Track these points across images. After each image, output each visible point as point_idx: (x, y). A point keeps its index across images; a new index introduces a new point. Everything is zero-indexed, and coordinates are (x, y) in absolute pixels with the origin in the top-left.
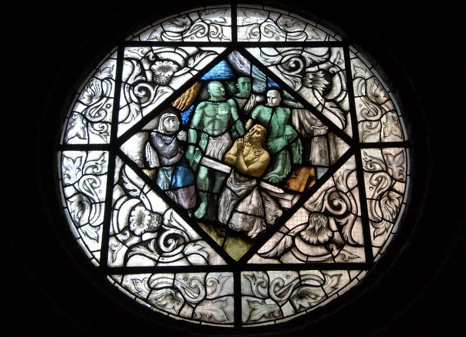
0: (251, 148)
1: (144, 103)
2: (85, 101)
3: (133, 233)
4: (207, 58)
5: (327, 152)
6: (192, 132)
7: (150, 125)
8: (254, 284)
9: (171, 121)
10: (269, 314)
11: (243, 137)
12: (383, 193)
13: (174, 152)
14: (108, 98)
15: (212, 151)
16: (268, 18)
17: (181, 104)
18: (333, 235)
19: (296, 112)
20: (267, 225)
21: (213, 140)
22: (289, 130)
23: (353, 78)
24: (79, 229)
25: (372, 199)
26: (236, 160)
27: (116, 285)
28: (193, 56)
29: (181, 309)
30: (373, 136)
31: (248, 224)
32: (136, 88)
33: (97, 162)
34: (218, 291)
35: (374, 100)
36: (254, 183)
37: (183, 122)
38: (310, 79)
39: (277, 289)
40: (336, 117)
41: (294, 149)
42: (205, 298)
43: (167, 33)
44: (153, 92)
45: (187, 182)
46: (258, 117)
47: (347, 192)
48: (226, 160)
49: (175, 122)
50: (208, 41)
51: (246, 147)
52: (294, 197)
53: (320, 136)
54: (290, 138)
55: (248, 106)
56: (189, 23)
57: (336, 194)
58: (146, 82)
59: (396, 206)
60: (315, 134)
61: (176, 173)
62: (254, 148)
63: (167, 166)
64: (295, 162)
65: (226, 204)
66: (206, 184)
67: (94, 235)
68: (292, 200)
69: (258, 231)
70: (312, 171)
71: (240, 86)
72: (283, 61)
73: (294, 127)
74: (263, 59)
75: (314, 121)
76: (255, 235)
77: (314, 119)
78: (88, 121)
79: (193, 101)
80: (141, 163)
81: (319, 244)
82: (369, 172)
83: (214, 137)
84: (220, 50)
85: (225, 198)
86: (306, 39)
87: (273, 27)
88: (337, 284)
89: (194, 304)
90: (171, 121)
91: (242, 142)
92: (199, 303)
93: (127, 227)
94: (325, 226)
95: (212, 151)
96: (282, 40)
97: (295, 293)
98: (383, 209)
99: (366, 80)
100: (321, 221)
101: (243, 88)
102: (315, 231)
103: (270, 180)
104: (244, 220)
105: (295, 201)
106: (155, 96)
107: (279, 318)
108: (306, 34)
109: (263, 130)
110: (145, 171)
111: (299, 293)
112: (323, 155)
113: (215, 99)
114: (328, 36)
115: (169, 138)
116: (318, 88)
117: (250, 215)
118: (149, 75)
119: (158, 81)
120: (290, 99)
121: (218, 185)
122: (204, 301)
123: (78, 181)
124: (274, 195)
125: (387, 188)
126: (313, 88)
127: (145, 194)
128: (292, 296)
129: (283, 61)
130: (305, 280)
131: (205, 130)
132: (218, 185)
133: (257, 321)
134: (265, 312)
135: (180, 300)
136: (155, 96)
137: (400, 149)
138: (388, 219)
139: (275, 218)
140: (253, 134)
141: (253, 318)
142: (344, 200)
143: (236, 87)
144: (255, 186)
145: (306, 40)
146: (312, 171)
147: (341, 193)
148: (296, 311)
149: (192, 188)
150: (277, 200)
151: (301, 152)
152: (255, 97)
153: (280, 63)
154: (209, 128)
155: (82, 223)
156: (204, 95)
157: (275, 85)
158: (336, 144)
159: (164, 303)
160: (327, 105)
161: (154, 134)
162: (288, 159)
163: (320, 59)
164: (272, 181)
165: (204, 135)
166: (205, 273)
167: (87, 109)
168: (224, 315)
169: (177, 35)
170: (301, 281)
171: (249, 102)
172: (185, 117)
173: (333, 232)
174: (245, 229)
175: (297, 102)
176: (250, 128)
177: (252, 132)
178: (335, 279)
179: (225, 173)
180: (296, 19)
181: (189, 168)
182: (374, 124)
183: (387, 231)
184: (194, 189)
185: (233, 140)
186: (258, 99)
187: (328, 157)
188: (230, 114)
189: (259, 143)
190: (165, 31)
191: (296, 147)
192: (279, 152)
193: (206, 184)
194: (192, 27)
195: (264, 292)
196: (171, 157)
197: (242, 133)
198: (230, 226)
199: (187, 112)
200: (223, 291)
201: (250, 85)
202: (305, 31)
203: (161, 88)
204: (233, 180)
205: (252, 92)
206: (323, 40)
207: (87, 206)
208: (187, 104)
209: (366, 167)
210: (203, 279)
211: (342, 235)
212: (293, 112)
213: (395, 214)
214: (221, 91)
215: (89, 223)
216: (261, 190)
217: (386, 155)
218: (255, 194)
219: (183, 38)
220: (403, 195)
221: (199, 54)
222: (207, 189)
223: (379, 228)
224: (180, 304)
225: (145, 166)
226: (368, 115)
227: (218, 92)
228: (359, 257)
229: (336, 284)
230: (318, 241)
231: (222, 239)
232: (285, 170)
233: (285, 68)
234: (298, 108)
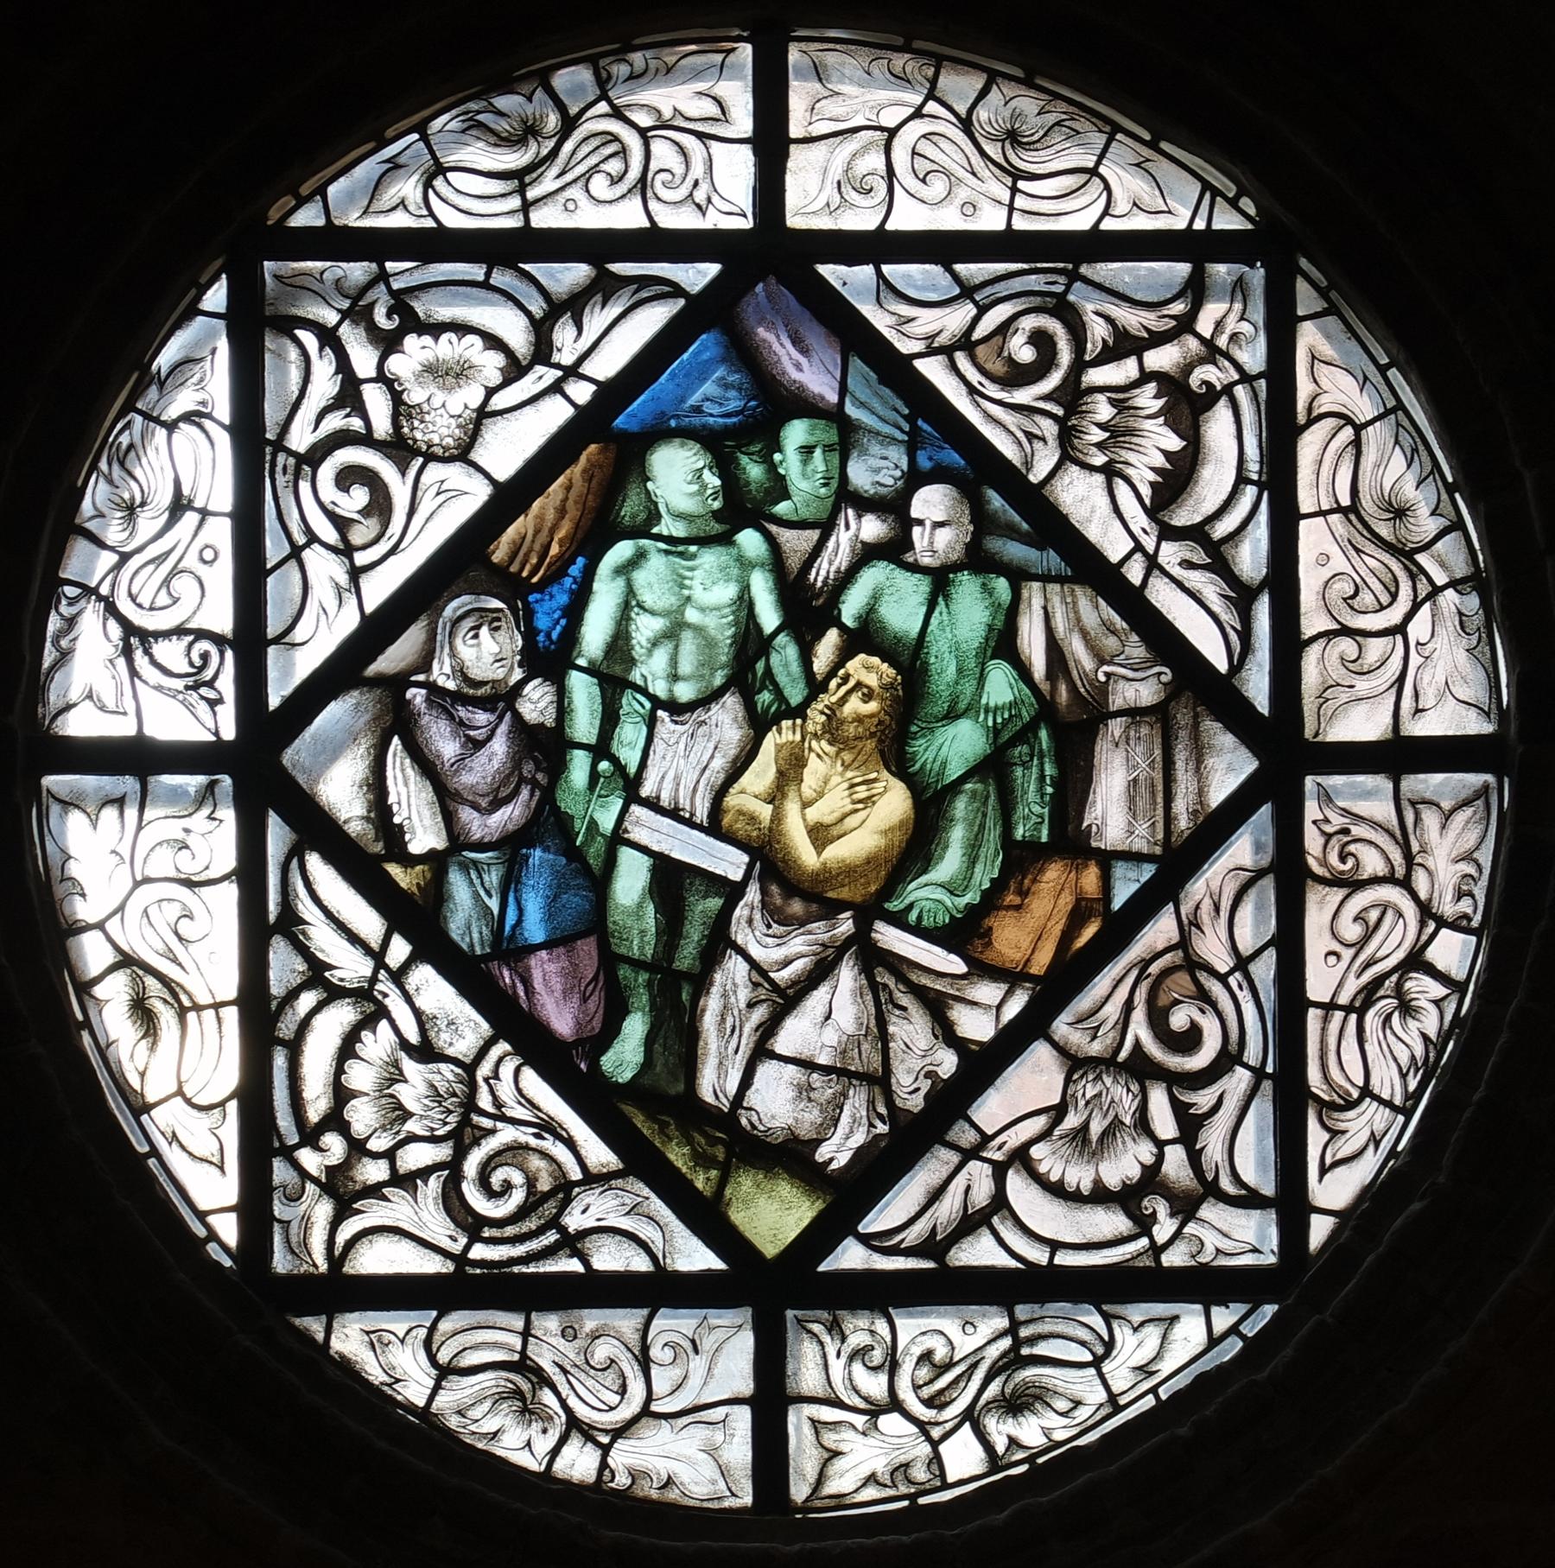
0: (833, 765)
1: (364, 547)
5: (1160, 787)
6: (582, 689)
7: (391, 660)
9: (484, 631)
10: (892, 1474)
11: (800, 712)
12: (1379, 981)
13: (505, 781)
14: (205, 513)
15: (671, 775)
16: (931, 96)
17: (530, 550)
18: (1160, 1158)
19: (1034, 593)
20: (895, 1114)
21: (673, 727)
22: (1000, 686)
23: (1301, 418)
24: (1123, 1401)
25: (1329, 1007)
26: (772, 821)
28: (573, 306)
29: (555, 1452)
30: (1362, 708)
31: (816, 1112)
32: (327, 471)
34: (695, 1381)
35: (1384, 530)
36: (846, 925)
37: (541, 638)
38: (1099, 425)
40: (1202, 612)
41: (1019, 772)
42: (646, 1412)
43: (449, 175)
44: (400, 492)
45: (567, 920)
46: (869, 618)
47: (1231, 972)
48: (726, 821)
49: (502, 636)
50: (647, 224)
51: (813, 760)
52: (1009, 993)
53: (1134, 713)
54: (1005, 722)
55: (825, 565)
56: (553, 121)
57: (1183, 978)
58: (366, 439)
59: (1425, 1037)
60: (1117, 702)
61: (518, 882)
62: (846, 767)
63: (481, 847)
64: (1019, 833)
65: (729, 1022)
66: (643, 932)
67: (208, 1148)
68: (999, 1007)
69: (859, 1139)
70: (1090, 879)
71: (789, 461)
72: (978, 334)
73: (1023, 671)
74: (891, 320)
75: (1111, 643)
76: (842, 1160)
77: (1114, 633)
78: (129, 628)
79: (579, 535)
80: (371, 835)
81: (1100, 1196)
82: (1335, 881)
83: (677, 709)
84: (698, 275)
85: (725, 995)
86: (1106, 213)
87: (953, 151)
88: (1158, 1357)
89: (606, 1431)
90: (484, 631)
91: (798, 737)
92: (620, 1432)
94: (1128, 1120)
95: (671, 775)
96: (992, 220)
97: (994, 1389)
98: (1372, 1049)
99: (1359, 428)
100: (1113, 1101)
101: (804, 475)
102: (1086, 1141)
103: (913, 916)
104: (804, 1091)
105: (1013, 1008)
107: (927, 1486)
108: (1107, 187)
109: (886, 680)
110: (394, 870)
111: (1008, 1391)
112: (1140, 804)
113: (678, 530)
114: (1208, 196)
115: (482, 718)
116: (1130, 471)
117: (826, 1070)
118: (376, 401)
119: (418, 435)
120: (1011, 532)
121: (694, 934)
122: (644, 1420)
123: (121, 908)
124: (926, 981)
125: (1400, 955)
126: (1110, 472)
128: (982, 1401)
129: (978, 334)
130: (1033, 1340)
131: (636, 676)
132: (694, 934)
133: (848, 1501)
134: (880, 1465)
135: (552, 1418)
137: (1475, 780)
138: (1385, 1096)
139: (926, 1085)
140: (843, 700)
141: (831, 1488)
142: (1213, 1005)
143: (772, 468)
144: (848, 942)
146: (1090, 879)
147: (1203, 977)
148: (995, 1462)
149: (587, 949)
150: (937, 1007)
151: (1049, 790)
152: (859, 517)
153: (965, 342)
154: (652, 670)
156: (630, 508)
157: (953, 458)
158: (1199, 754)
159: (489, 1426)
160: (1170, 554)
161: (416, 696)
162: (989, 823)
163: (1150, 319)
164: (920, 918)
165: (631, 703)
166: (645, 1312)
167: (118, 567)
168: (718, 1476)
169: (496, 186)
170: (1018, 1343)
171: (831, 544)
172: (548, 611)
173: (1160, 1145)
174: (805, 1132)
175: (1041, 548)
176: (832, 674)
177: (844, 689)
178: (1152, 1334)
179: (722, 880)
180: (1063, 106)
181: (574, 854)
182: (1375, 648)
183: (1377, 1144)
184: (595, 954)
185: (759, 724)
186: (872, 528)
187: (1160, 811)
188: (745, 603)
189: (870, 745)
190: (439, 170)
191: (1026, 765)
192: (955, 787)
193: (643, 932)
194: (568, 146)
195: (875, 1386)
196: (497, 804)
197: (795, 695)
198: (744, 1122)
199: (555, 589)
200: (712, 1384)
201: (836, 461)
202: (1102, 170)
203: (435, 472)
204: (757, 916)
205: (846, 497)
206: (1181, 225)
207: (166, 1017)
208: (555, 549)
209: (1324, 862)
210: (637, 1336)
211: (1195, 1158)
212: (1025, 594)
213: (1417, 1070)
214: (704, 487)
215: (180, 1092)
216: (873, 959)
217: (1413, 803)
218: (847, 975)
219: (526, 207)
220: (1458, 987)
222: (649, 951)
223: (1344, 1132)
224: (551, 1432)
225: (386, 847)
226: (1355, 603)
227: (692, 495)
229: (1152, 1355)
230: (1098, 1183)
231: (714, 1173)
232: (979, 868)
233: (988, 366)
234: (1046, 578)
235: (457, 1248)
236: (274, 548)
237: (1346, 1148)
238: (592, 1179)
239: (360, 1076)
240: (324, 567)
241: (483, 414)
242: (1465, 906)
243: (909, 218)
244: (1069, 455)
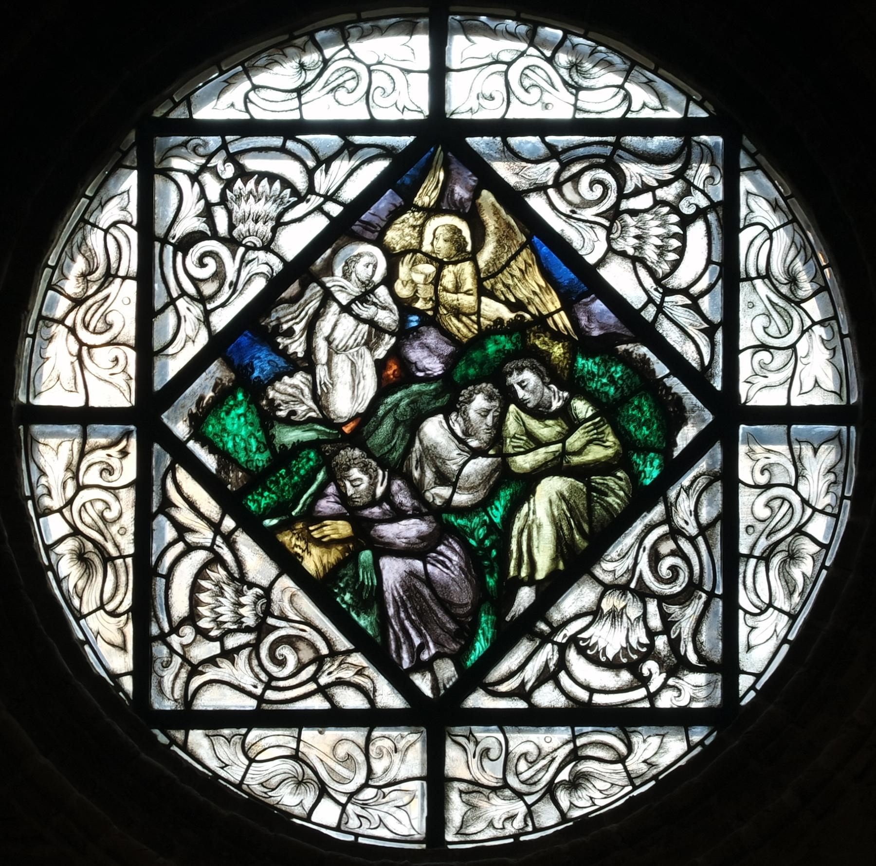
2: (72, 286)
4: (365, 168)
8: (474, 757)
27: (175, 748)
67: (118, 640)
99: (771, 232)
145: (626, 113)
155: (85, 611)
228: (398, 807)
235: (258, 691)
236: (159, 301)
238: (541, 188)
240: (190, 311)
243: (517, 112)
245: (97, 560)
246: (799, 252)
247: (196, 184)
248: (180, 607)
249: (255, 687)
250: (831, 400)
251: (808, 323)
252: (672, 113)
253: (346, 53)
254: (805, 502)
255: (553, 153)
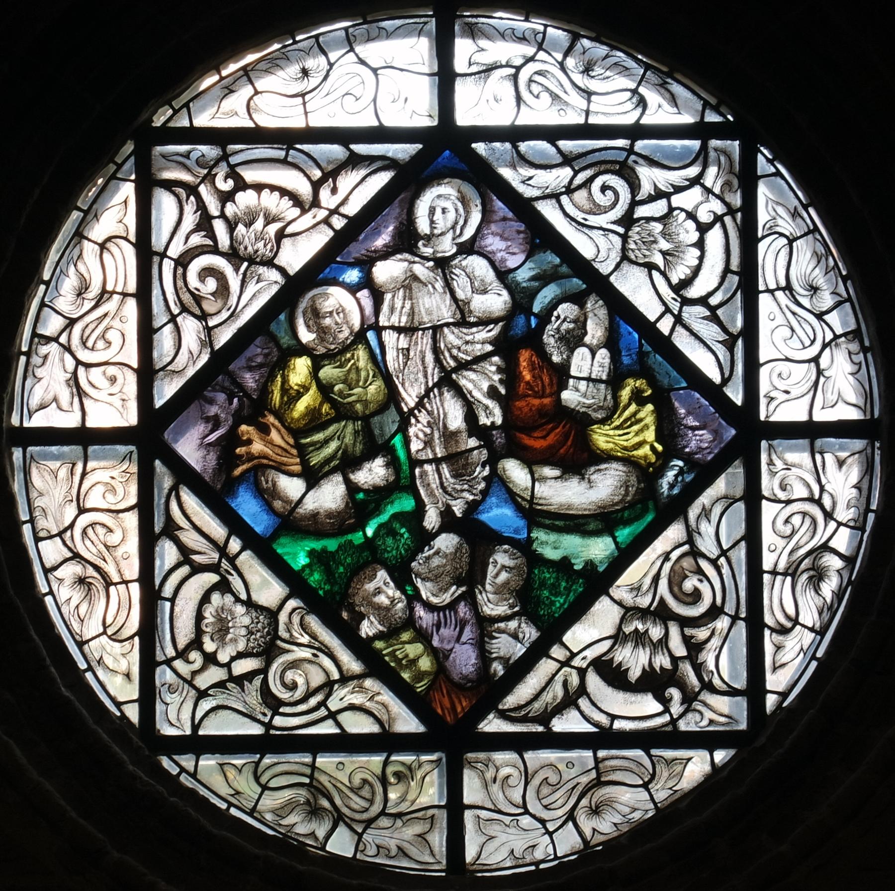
3: (210, 659)
33: (786, 396)
39: (545, 790)
84: (736, 394)
93: (196, 643)
106: (656, 579)
127: (668, 310)
136: (656, 579)
211: (698, 668)
220: (323, 848)
221: (351, 166)
237: (231, 773)
239: (271, 201)
241: (249, 604)
242: (371, 851)
243: (527, 118)
244: (630, 612)
245: (99, 584)
246: (819, 262)
247: (688, 183)
248: (715, 237)
249: (635, 162)
250: (853, 414)
251: (829, 336)
252: (687, 119)
253: (351, 56)
254: (68, 349)
255: (567, 160)
